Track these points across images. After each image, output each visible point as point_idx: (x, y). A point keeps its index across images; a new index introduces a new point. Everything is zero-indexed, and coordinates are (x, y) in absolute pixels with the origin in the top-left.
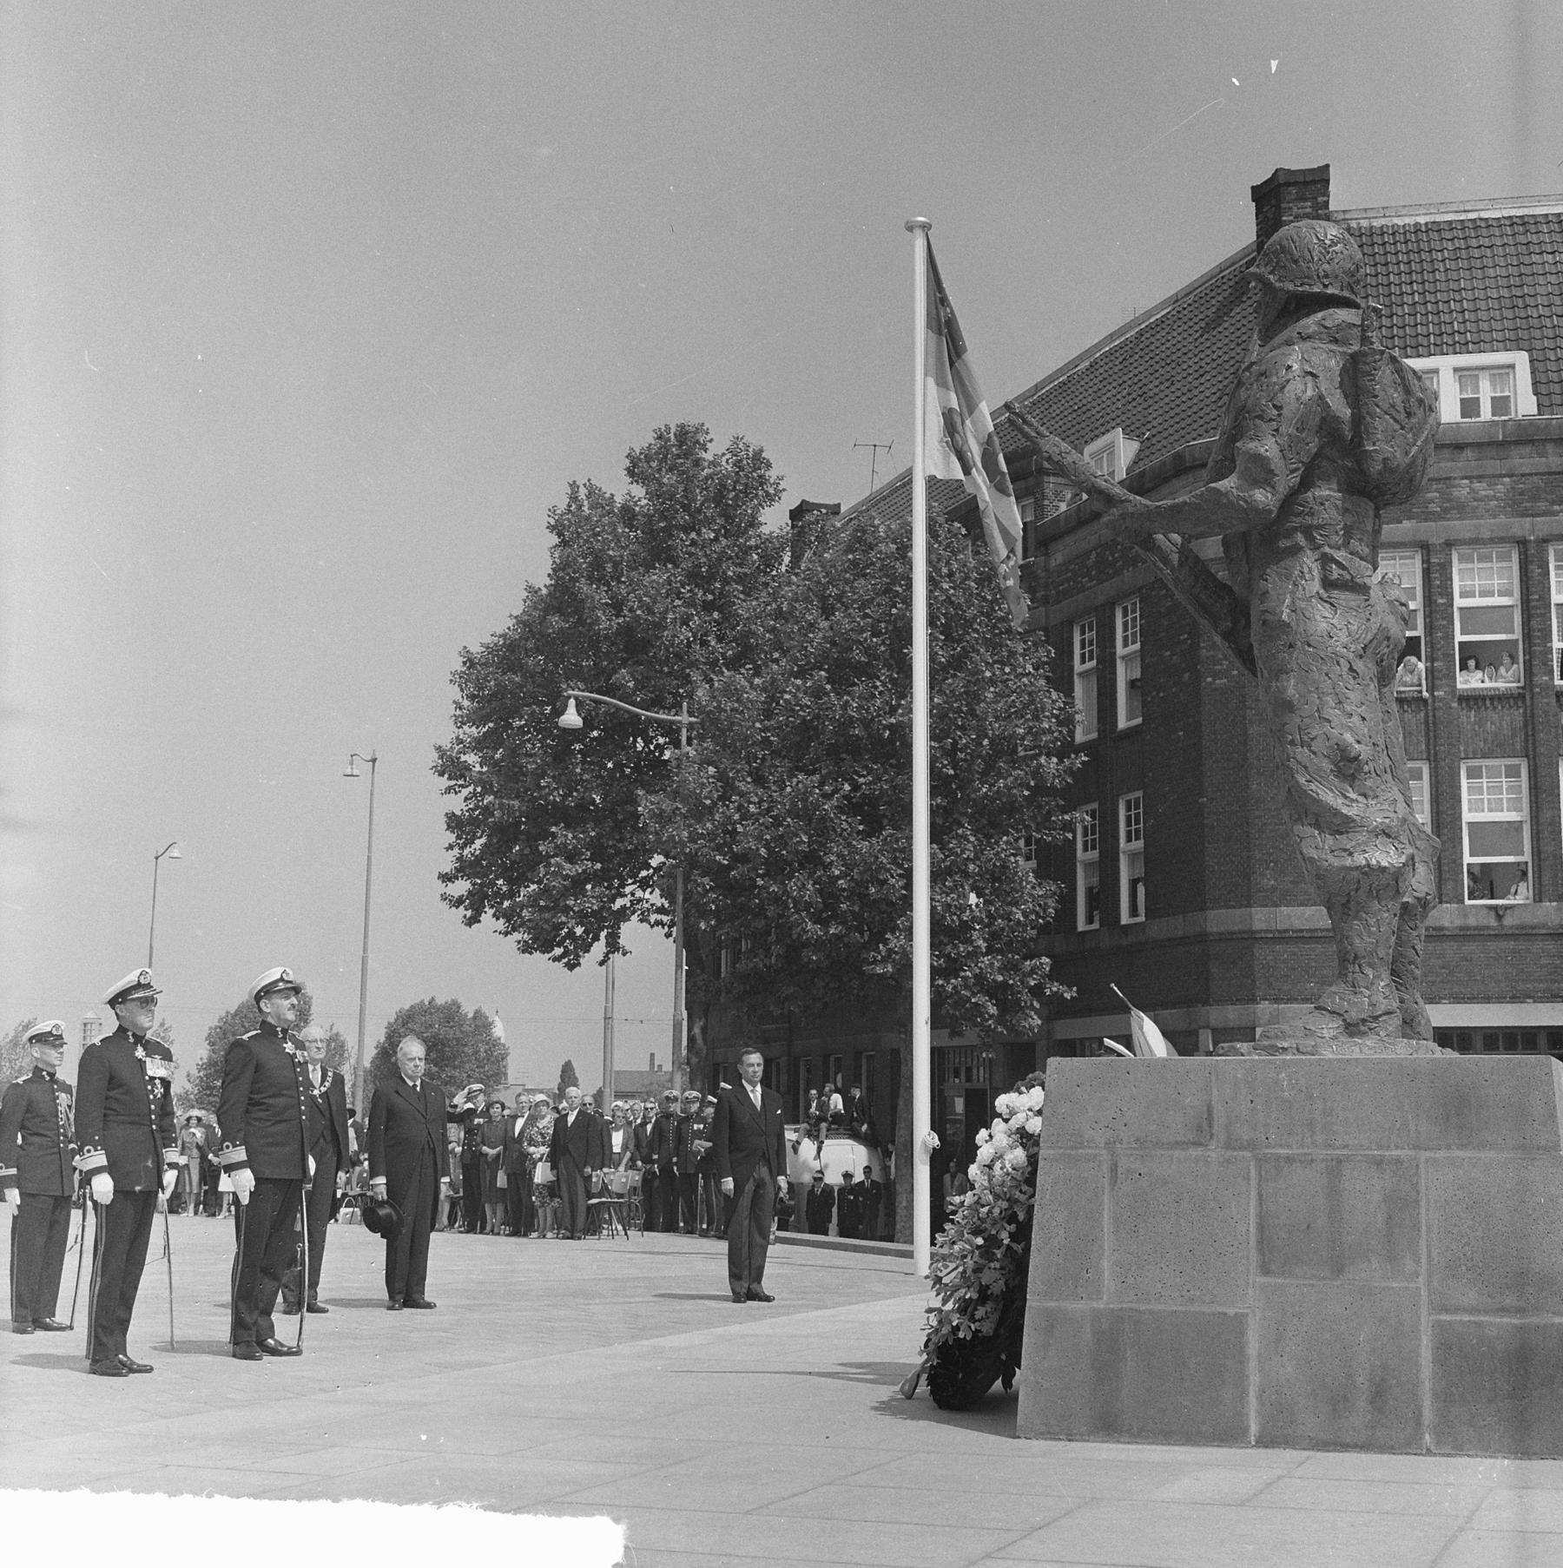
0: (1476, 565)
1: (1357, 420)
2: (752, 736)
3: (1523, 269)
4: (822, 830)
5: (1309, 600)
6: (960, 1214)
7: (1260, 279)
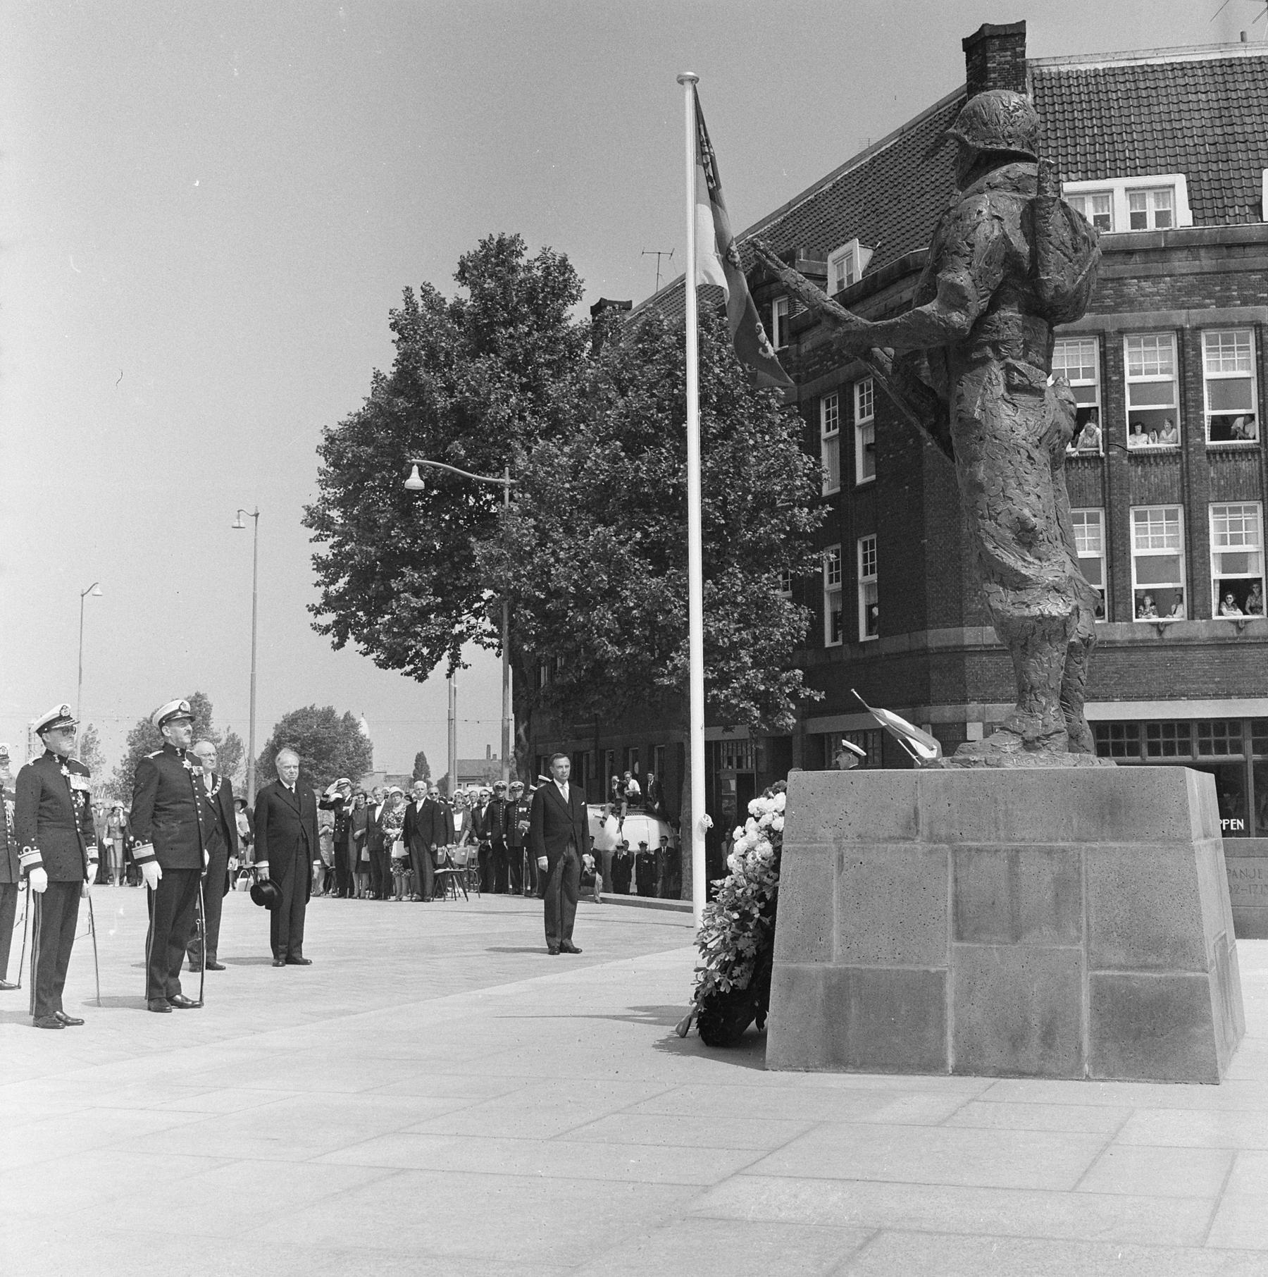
0: (1143, 348)
1: (1034, 255)
2: (562, 495)
3: (1183, 107)
4: (619, 570)
5: (995, 401)
6: (720, 895)
7: (957, 138)
